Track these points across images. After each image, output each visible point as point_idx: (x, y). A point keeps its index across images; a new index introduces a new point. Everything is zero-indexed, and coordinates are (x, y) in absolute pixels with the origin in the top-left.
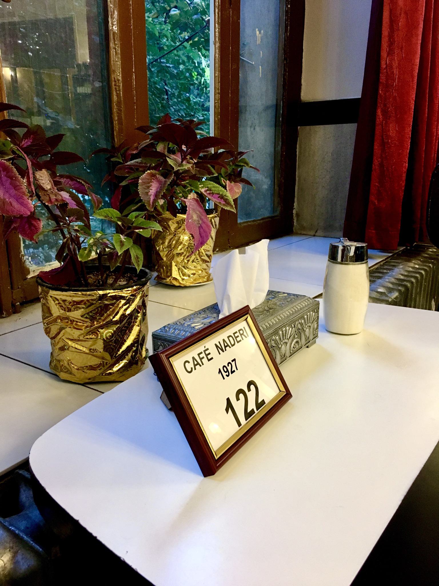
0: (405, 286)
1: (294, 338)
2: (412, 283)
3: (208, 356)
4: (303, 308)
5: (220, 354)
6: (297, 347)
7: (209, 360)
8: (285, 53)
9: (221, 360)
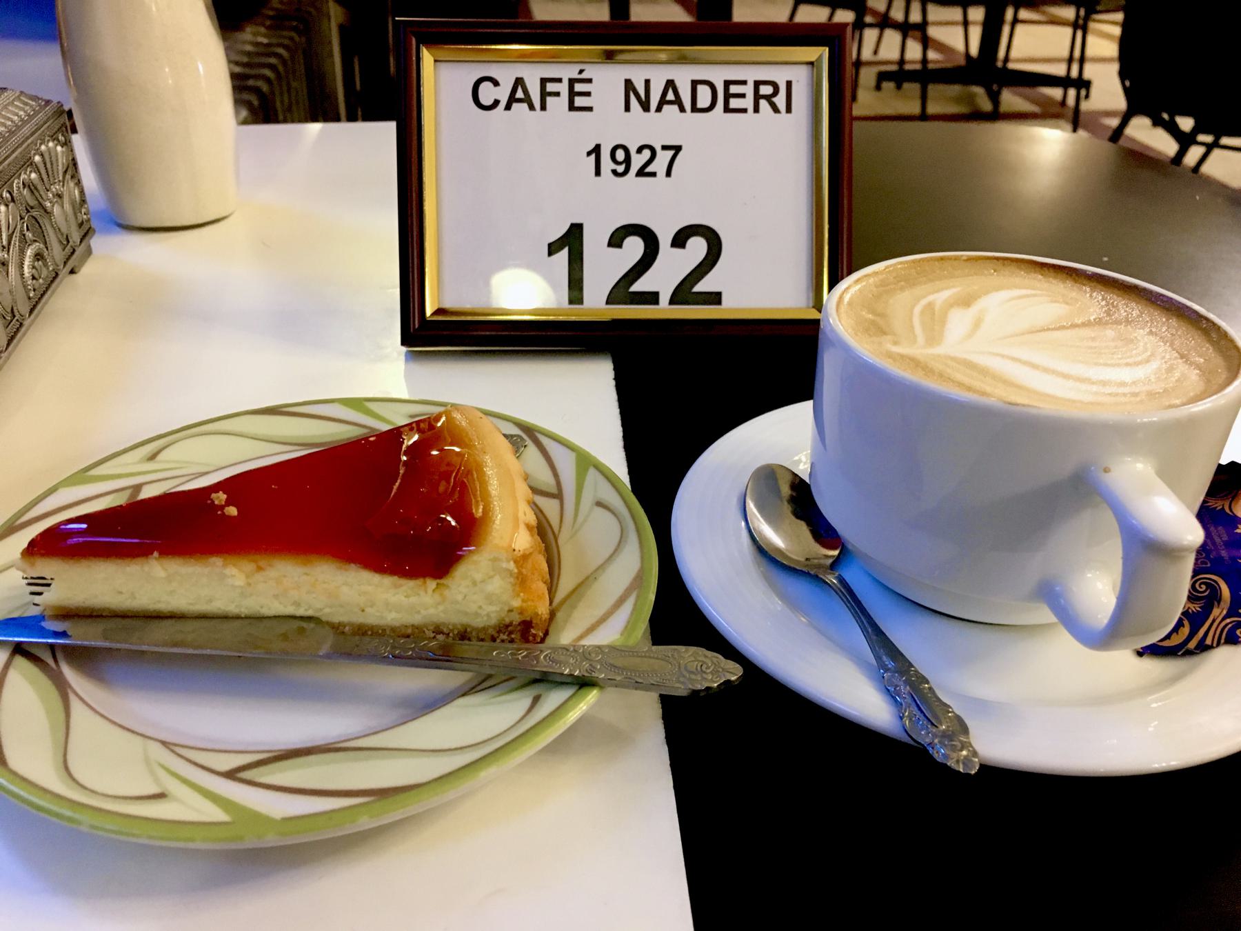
0: (256, 91)
1: (24, 242)
2: (268, 80)
4: (19, 128)
5: (590, 109)
6: (44, 273)
9: (612, 122)
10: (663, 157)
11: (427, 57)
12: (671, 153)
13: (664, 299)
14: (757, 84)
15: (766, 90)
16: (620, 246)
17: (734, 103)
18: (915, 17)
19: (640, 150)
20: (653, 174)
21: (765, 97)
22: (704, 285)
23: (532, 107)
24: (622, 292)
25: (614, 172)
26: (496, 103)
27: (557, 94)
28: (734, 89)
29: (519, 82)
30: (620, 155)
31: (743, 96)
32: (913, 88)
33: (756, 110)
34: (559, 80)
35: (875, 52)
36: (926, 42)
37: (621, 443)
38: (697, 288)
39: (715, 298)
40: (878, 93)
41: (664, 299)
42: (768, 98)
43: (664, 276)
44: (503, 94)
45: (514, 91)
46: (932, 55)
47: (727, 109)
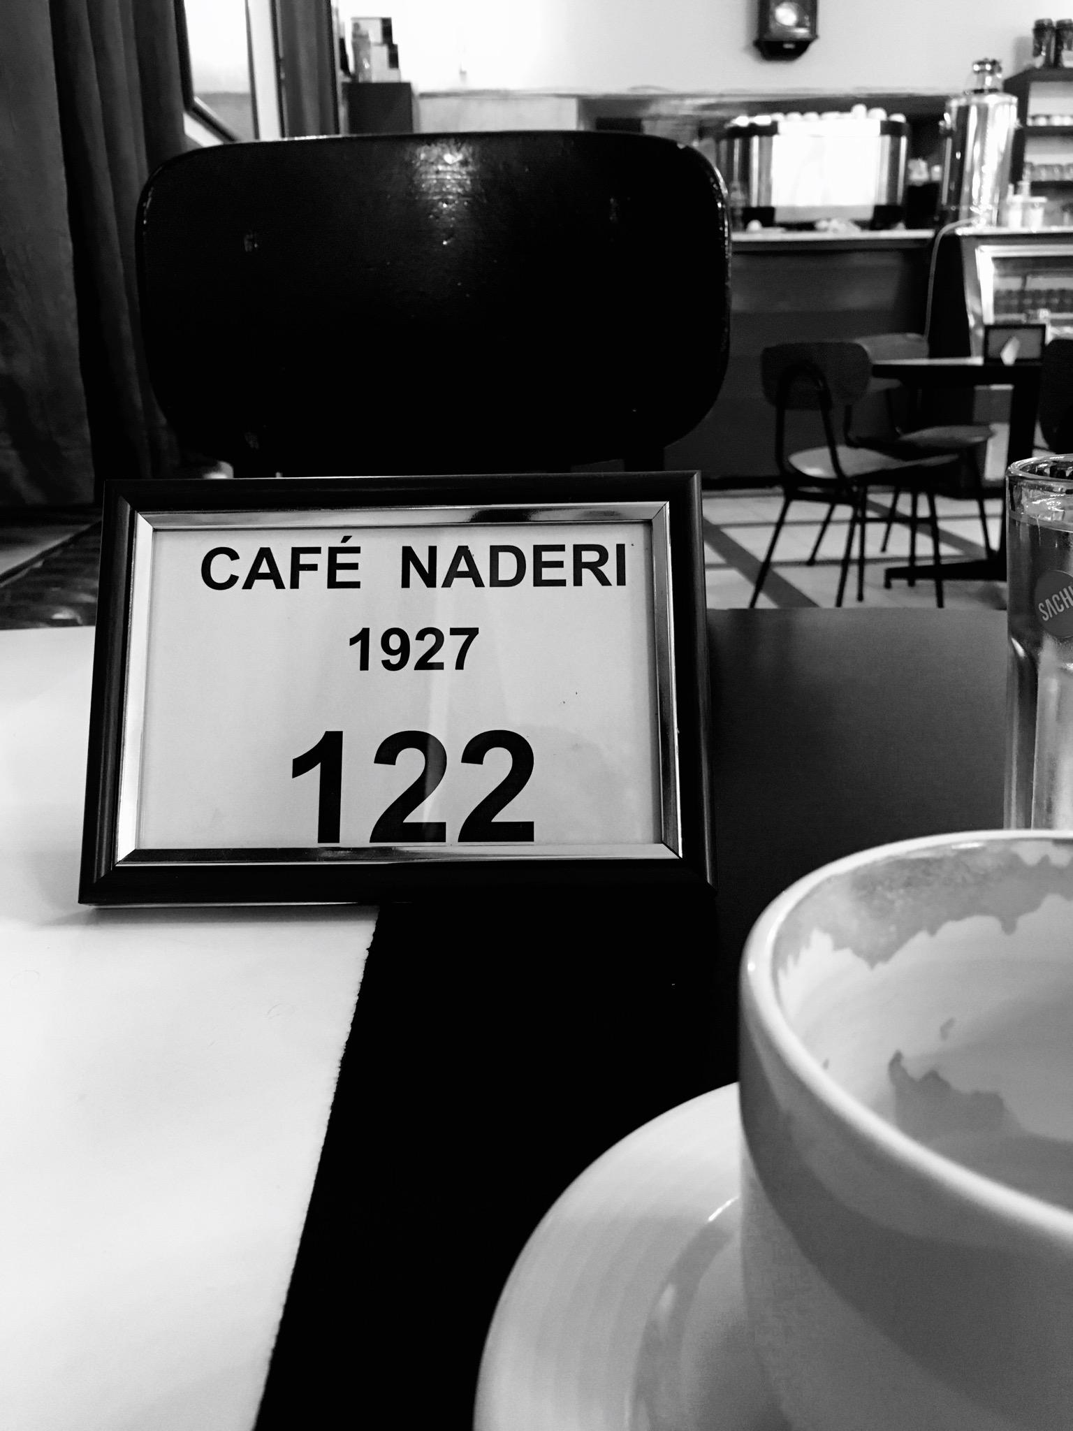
3: (339, 572)
5: (356, 585)
7: (332, 583)
8: (968, 1201)
9: (382, 598)
10: (453, 644)
11: (144, 527)
12: (462, 639)
13: (453, 832)
14: (578, 549)
15: (590, 557)
16: (479, 761)
17: (547, 574)
18: (923, 512)
19: (421, 636)
20: (440, 666)
21: (589, 565)
22: (507, 815)
23: (279, 585)
24: (393, 823)
25: (387, 664)
26: (233, 579)
27: (313, 567)
28: (547, 556)
29: (265, 554)
30: (395, 642)
31: (559, 564)
32: (927, 585)
33: (578, 581)
34: (317, 550)
35: (884, 549)
36: (937, 536)
37: (339, 1054)
38: (499, 818)
39: (523, 832)
40: (886, 591)
41: (453, 832)
42: (593, 567)
43: (449, 804)
44: (242, 569)
45: (257, 564)
46: (945, 550)
47: (538, 582)
